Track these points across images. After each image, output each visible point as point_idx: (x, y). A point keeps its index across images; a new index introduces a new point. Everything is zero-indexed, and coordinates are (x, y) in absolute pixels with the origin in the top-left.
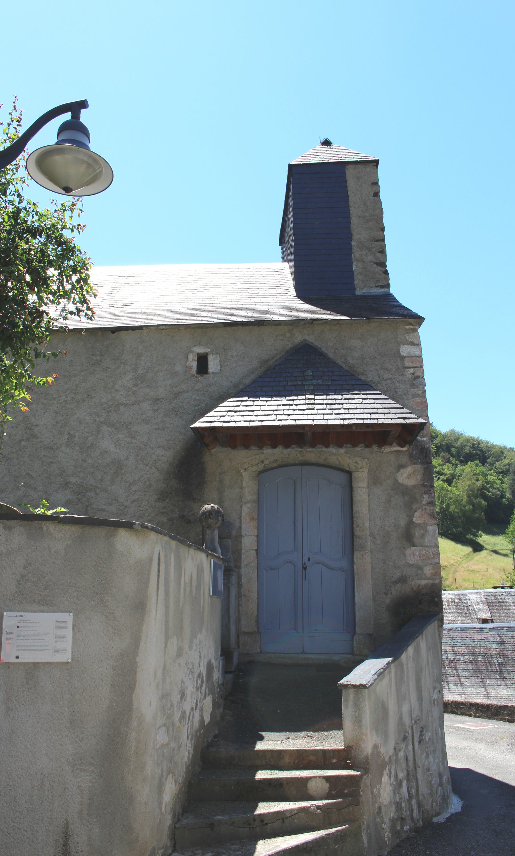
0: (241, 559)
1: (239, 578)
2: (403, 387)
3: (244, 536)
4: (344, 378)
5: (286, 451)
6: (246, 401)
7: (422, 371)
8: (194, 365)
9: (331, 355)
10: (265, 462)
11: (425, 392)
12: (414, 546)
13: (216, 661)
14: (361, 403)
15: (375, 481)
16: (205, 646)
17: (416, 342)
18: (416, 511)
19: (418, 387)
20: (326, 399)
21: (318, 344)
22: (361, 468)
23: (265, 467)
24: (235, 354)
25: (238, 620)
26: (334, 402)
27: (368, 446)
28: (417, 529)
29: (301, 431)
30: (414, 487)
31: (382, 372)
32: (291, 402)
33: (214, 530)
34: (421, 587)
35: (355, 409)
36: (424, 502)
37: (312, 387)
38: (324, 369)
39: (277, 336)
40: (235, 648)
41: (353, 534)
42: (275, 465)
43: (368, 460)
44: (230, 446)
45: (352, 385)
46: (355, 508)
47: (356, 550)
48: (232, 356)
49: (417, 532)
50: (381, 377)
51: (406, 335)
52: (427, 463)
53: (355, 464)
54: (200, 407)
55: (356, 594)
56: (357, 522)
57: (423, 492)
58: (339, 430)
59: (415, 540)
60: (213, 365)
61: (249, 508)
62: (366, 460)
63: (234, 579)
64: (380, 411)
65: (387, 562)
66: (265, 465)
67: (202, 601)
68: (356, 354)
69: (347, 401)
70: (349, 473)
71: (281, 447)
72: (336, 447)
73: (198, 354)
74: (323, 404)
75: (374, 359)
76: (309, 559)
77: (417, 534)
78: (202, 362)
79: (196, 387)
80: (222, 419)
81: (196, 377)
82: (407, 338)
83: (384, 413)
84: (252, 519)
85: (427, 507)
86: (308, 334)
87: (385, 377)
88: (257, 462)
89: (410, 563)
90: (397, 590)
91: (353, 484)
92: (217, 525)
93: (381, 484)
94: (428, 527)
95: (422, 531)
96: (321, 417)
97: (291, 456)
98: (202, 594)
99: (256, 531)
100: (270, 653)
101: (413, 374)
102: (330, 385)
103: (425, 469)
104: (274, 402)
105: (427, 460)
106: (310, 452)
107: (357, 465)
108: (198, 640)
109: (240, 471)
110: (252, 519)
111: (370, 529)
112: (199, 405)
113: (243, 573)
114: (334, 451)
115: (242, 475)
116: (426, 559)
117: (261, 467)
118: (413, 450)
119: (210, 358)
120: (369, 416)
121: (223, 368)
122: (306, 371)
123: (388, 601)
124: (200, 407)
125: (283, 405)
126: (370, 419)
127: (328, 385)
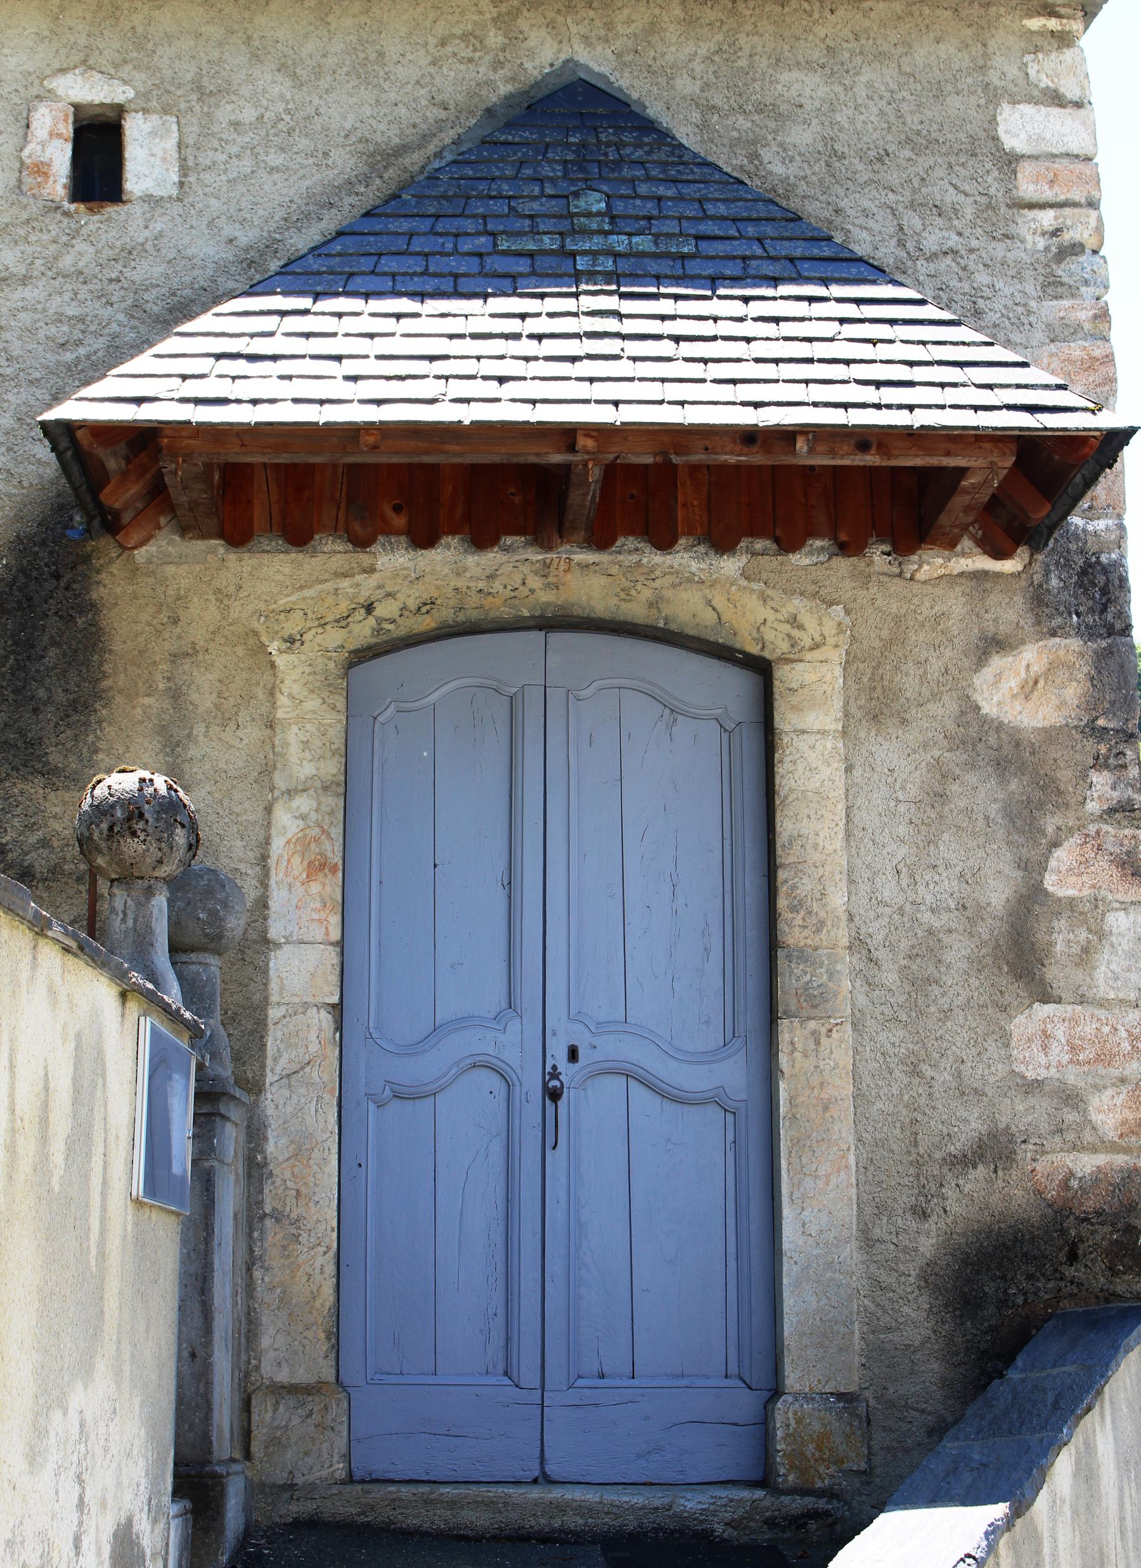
0: (263, 1047)
1: (255, 1133)
2: (1007, 291)
3: (278, 946)
4: (751, 230)
5: (478, 563)
6: (305, 312)
7: (1093, 223)
8: (60, 157)
9: (686, 135)
10: (381, 610)
11: (1103, 315)
12: (1046, 999)
13: (155, 1521)
14: (832, 340)
15: (875, 704)
16: (106, 1450)
17: (1070, 91)
18: (1056, 844)
19: (1073, 292)
20: (673, 317)
21: (629, 83)
22: (816, 646)
23: (378, 631)
24: (248, 115)
25: (249, 1330)
26: (707, 328)
27: (849, 547)
28: (1062, 924)
29: (557, 458)
30: (1050, 735)
31: (917, 222)
32: (513, 326)
33: (149, 892)
34: (1074, 1184)
35: (810, 361)
36: (1093, 807)
37: (609, 264)
38: (661, 191)
39: (443, 43)
40: (232, 1460)
41: (772, 944)
42: (425, 623)
43: (848, 612)
44: (221, 535)
45: (791, 260)
46: (785, 827)
47: (788, 1015)
48: (236, 125)
49: (1063, 939)
50: (910, 245)
51: (1028, 58)
52: (1111, 631)
53: (786, 628)
54: (82, 351)
55: (787, 1212)
56: (794, 887)
57: (1091, 762)
58: (732, 459)
59: (1053, 973)
60: (147, 160)
61: (304, 817)
62: (840, 608)
63: (231, 1138)
64: (919, 374)
65: (924, 1067)
66: (380, 621)
67: (95, 1223)
68: (801, 137)
69: (770, 329)
70: (761, 670)
71: (453, 541)
72: (702, 549)
73: (77, 107)
74: (658, 337)
75: (879, 159)
76: (573, 1054)
77: (1059, 947)
78: (98, 149)
79: (67, 262)
80: (193, 389)
81: (66, 214)
82: (1032, 72)
83: (942, 385)
84: (317, 867)
85: (1105, 828)
86: (586, 39)
87: (931, 242)
88: (344, 607)
89: (1030, 1075)
90: (970, 1198)
91: (777, 717)
92: (165, 870)
93: (904, 722)
94: (1110, 918)
95: (1083, 935)
96: (654, 391)
97: (497, 586)
98: (96, 1181)
99: (335, 920)
100: (392, 1482)
101: (1056, 232)
102: (692, 256)
103: (1103, 658)
104: (437, 319)
105: (1110, 617)
106: (584, 567)
107: (795, 633)
108: (74, 1419)
109: (263, 646)
110: (317, 867)
111: (851, 918)
112: (79, 343)
113: (270, 1111)
114: (694, 566)
115: (273, 665)
116: (1098, 1059)
117: (362, 631)
118: (1047, 573)
119: (135, 128)
120: (870, 394)
121: (192, 178)
122: (576, 195)
123: (927, 1245)
124: (82, 351)
125: (475, 336)
126: (878, 406)
127: (684, 257)
